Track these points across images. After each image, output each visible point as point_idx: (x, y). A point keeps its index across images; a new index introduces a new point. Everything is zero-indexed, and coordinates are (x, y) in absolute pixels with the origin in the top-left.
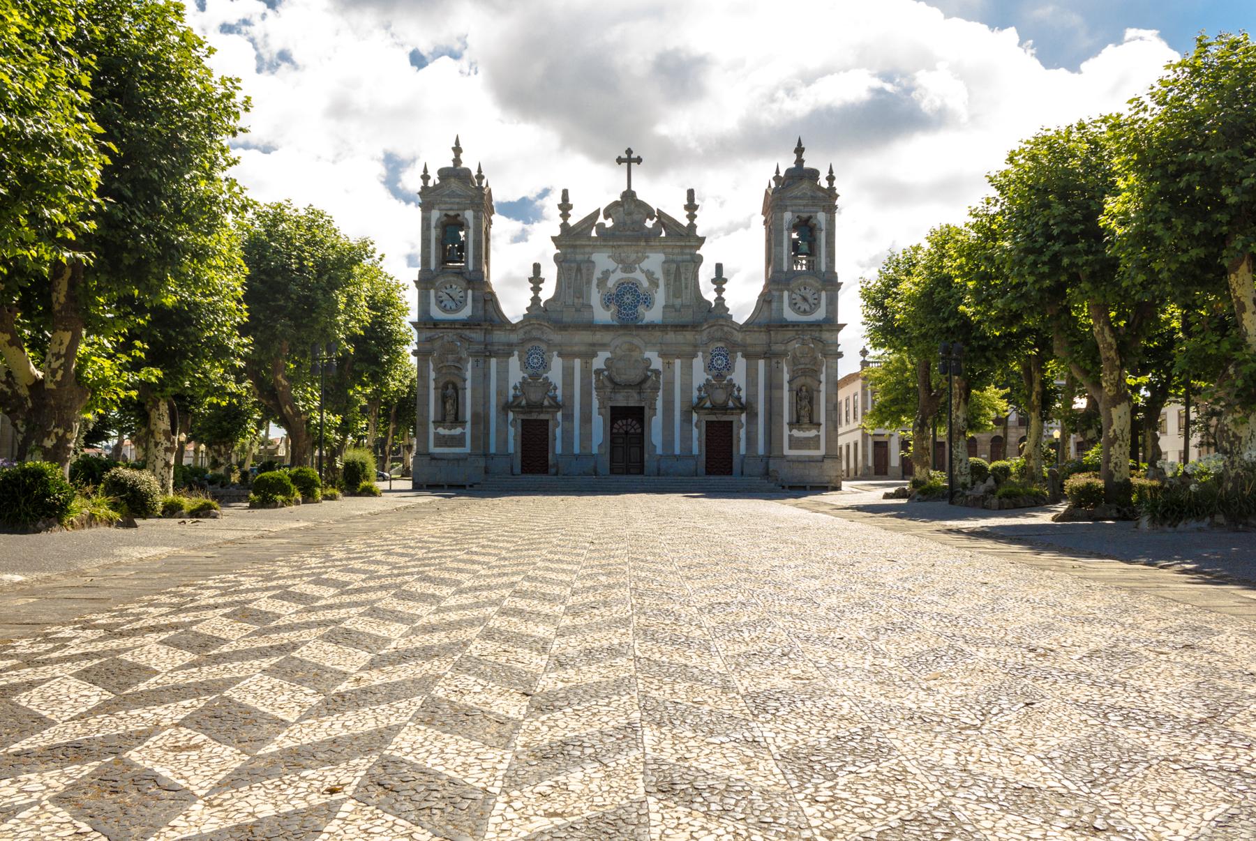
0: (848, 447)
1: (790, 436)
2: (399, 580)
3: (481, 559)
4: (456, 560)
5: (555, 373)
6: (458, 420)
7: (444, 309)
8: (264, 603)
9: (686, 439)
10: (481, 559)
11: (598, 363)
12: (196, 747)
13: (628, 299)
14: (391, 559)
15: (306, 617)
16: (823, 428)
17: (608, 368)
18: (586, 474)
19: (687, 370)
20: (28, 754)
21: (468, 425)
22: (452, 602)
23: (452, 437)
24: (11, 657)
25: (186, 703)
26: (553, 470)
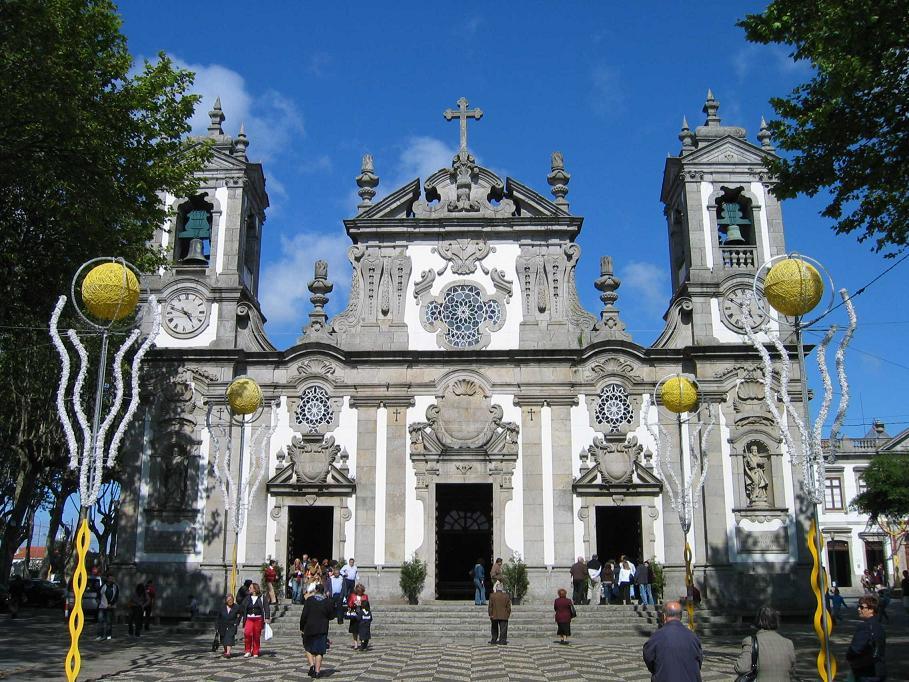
5: (345, 429)
7: (174, 333)
11: (416, 414)
17: (431, 422)
19: (563, 425)
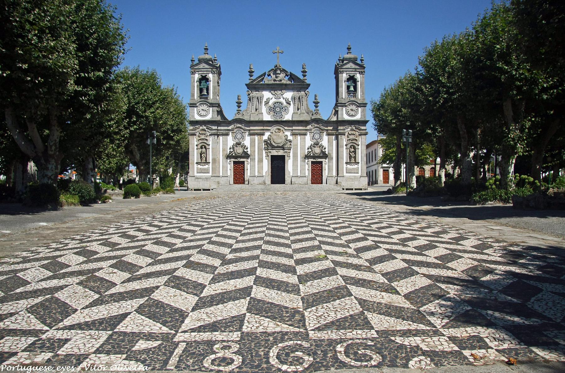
0: (372, 171)
1: (346, 168)
2: (180, 225)
3: (212, 217)
4: (202, 218)
6: (207, 163)
8: (132, 232)
9: (303, 169)
10: (212, 217)
12: (115, 273)
13: (278, 110)
14: (178, 218)
15: (146, 237)
16: (360, 164)
18: (260, 184)
20: (66, 273)
21: (211, 164)
22: (199, 232)
23: (204, 169)
24: (51, 248)
25: (110, 261)
26: (247, 183)
